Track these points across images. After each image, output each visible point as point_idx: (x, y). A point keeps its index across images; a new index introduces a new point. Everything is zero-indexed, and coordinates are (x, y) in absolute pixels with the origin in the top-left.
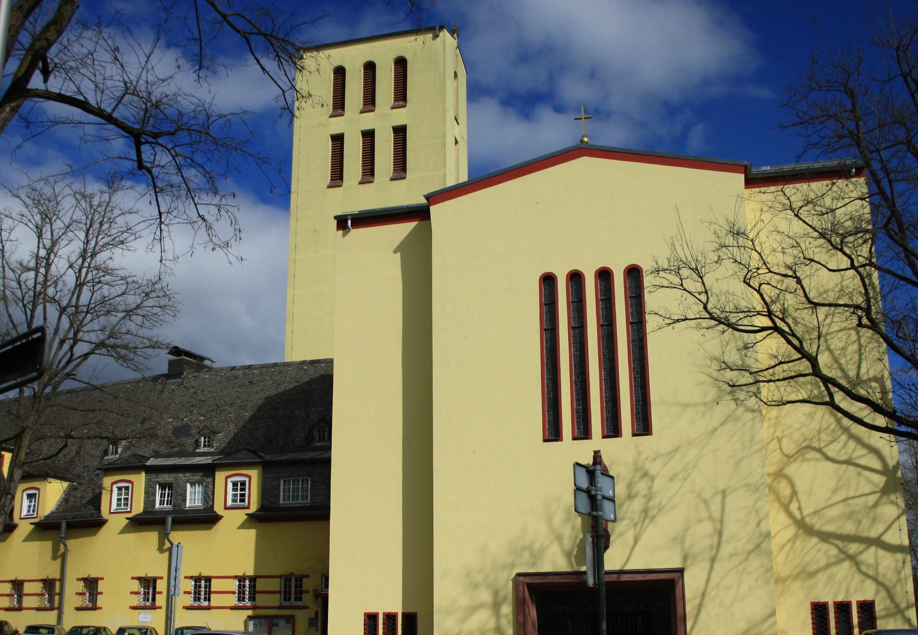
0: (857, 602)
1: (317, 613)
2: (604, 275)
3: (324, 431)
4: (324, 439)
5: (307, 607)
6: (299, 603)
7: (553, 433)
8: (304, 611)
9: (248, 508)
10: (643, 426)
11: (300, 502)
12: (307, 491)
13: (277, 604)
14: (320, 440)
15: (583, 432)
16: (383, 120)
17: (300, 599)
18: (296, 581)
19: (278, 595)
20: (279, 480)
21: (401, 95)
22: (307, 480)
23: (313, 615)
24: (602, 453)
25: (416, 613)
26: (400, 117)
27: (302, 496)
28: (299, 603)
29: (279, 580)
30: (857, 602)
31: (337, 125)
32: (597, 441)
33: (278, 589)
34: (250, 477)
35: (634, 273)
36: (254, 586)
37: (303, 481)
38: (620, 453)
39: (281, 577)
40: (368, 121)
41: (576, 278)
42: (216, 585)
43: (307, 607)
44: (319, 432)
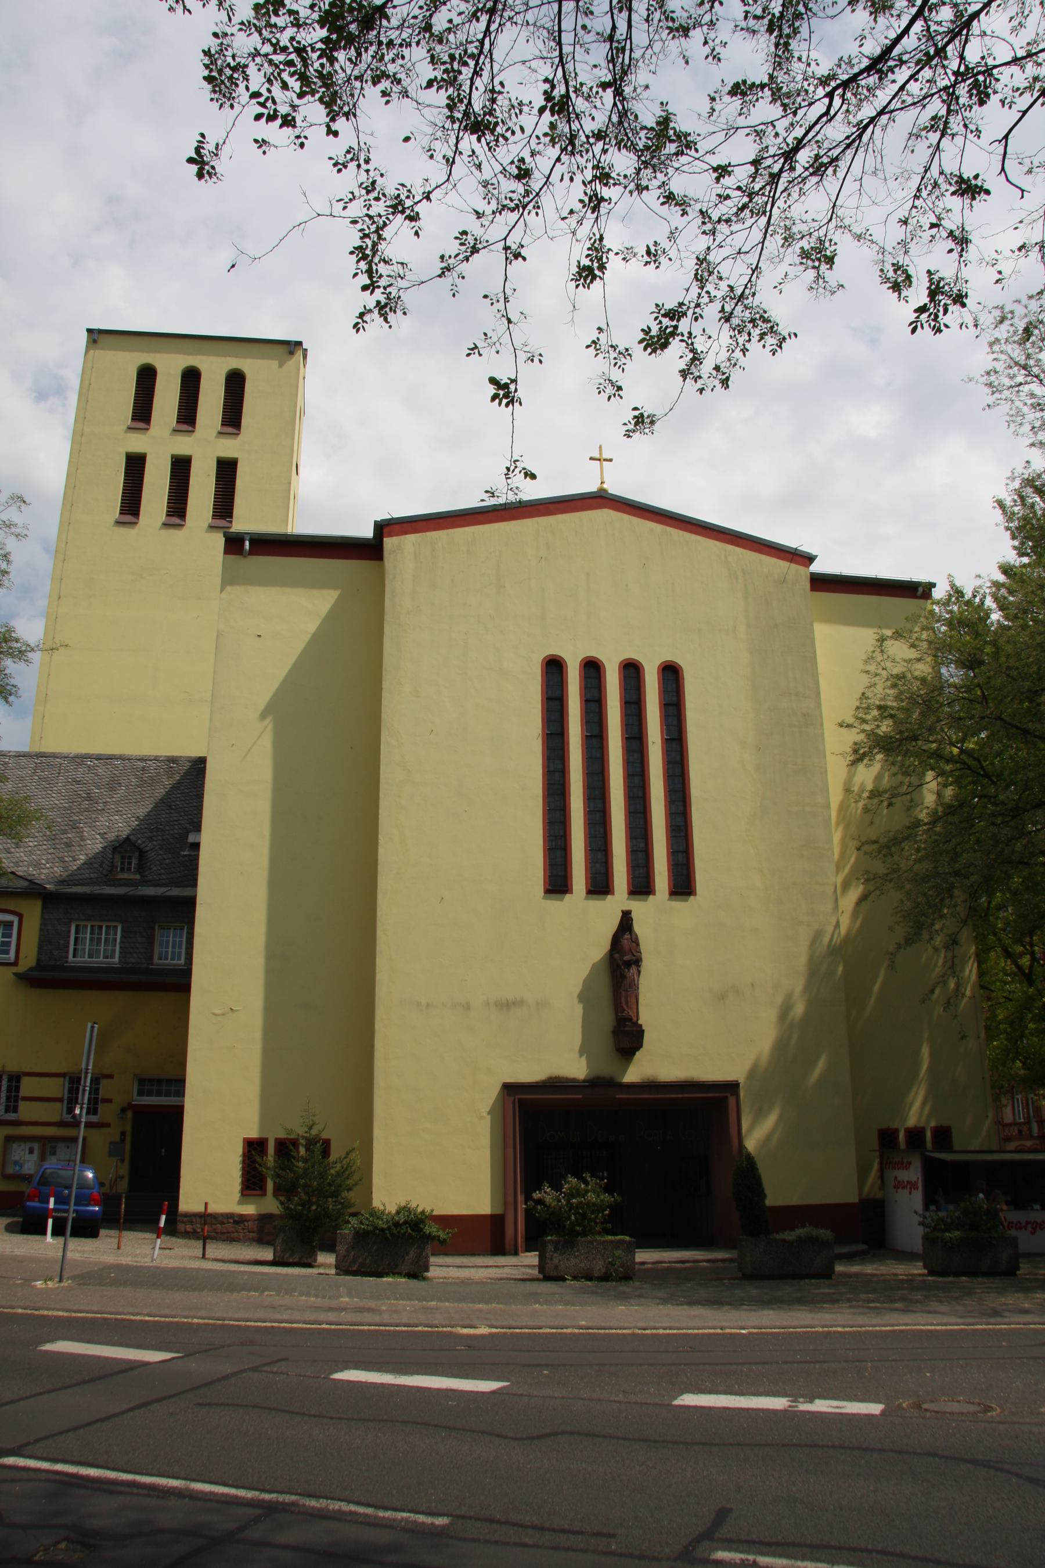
0: (276, 1139)
1: (123, 1134)
2: (632, 670)
3: (130, 858)
4: (129, 869)
5: (108, 1125)
6: (12, 1116)
7: (557, 883)
8: (104, 1130)
9: (15, 964)
10: (683, 886)
11: (100, 960)
12: (180, 947)
13: (56, 1118)
14: (122, 870)
15: (600, 886)
16: (205, 446)
17: (15, 1110)
18: (10, 1080)
19: (59, 1104)
20: (69, 924)
21: (233, 417)
22: (116, 928)
23: (117, 1138)
24: (633, 915)
25: (245, 1139)
26: (228, 448)
27: (173, 953)
28: (12, 1116)
29: (61, 1079)
30: (276, 1139)
31: (137, 443)
32: (619, 899)
33: (60, 1095)
34: (20, 916)
35: (671, 673)
36: (97, 1091)
37: (108, 927)
38: (656, 917)
39: (63, 1075)
40: (183, 445)
41: (632, 670)
42: (27, 1086)
43: (108, 1125)
44: (123, 858)
